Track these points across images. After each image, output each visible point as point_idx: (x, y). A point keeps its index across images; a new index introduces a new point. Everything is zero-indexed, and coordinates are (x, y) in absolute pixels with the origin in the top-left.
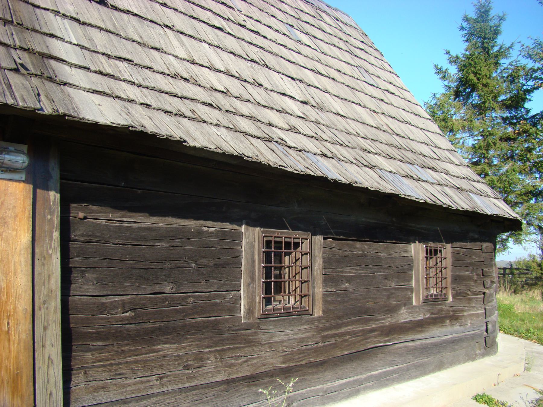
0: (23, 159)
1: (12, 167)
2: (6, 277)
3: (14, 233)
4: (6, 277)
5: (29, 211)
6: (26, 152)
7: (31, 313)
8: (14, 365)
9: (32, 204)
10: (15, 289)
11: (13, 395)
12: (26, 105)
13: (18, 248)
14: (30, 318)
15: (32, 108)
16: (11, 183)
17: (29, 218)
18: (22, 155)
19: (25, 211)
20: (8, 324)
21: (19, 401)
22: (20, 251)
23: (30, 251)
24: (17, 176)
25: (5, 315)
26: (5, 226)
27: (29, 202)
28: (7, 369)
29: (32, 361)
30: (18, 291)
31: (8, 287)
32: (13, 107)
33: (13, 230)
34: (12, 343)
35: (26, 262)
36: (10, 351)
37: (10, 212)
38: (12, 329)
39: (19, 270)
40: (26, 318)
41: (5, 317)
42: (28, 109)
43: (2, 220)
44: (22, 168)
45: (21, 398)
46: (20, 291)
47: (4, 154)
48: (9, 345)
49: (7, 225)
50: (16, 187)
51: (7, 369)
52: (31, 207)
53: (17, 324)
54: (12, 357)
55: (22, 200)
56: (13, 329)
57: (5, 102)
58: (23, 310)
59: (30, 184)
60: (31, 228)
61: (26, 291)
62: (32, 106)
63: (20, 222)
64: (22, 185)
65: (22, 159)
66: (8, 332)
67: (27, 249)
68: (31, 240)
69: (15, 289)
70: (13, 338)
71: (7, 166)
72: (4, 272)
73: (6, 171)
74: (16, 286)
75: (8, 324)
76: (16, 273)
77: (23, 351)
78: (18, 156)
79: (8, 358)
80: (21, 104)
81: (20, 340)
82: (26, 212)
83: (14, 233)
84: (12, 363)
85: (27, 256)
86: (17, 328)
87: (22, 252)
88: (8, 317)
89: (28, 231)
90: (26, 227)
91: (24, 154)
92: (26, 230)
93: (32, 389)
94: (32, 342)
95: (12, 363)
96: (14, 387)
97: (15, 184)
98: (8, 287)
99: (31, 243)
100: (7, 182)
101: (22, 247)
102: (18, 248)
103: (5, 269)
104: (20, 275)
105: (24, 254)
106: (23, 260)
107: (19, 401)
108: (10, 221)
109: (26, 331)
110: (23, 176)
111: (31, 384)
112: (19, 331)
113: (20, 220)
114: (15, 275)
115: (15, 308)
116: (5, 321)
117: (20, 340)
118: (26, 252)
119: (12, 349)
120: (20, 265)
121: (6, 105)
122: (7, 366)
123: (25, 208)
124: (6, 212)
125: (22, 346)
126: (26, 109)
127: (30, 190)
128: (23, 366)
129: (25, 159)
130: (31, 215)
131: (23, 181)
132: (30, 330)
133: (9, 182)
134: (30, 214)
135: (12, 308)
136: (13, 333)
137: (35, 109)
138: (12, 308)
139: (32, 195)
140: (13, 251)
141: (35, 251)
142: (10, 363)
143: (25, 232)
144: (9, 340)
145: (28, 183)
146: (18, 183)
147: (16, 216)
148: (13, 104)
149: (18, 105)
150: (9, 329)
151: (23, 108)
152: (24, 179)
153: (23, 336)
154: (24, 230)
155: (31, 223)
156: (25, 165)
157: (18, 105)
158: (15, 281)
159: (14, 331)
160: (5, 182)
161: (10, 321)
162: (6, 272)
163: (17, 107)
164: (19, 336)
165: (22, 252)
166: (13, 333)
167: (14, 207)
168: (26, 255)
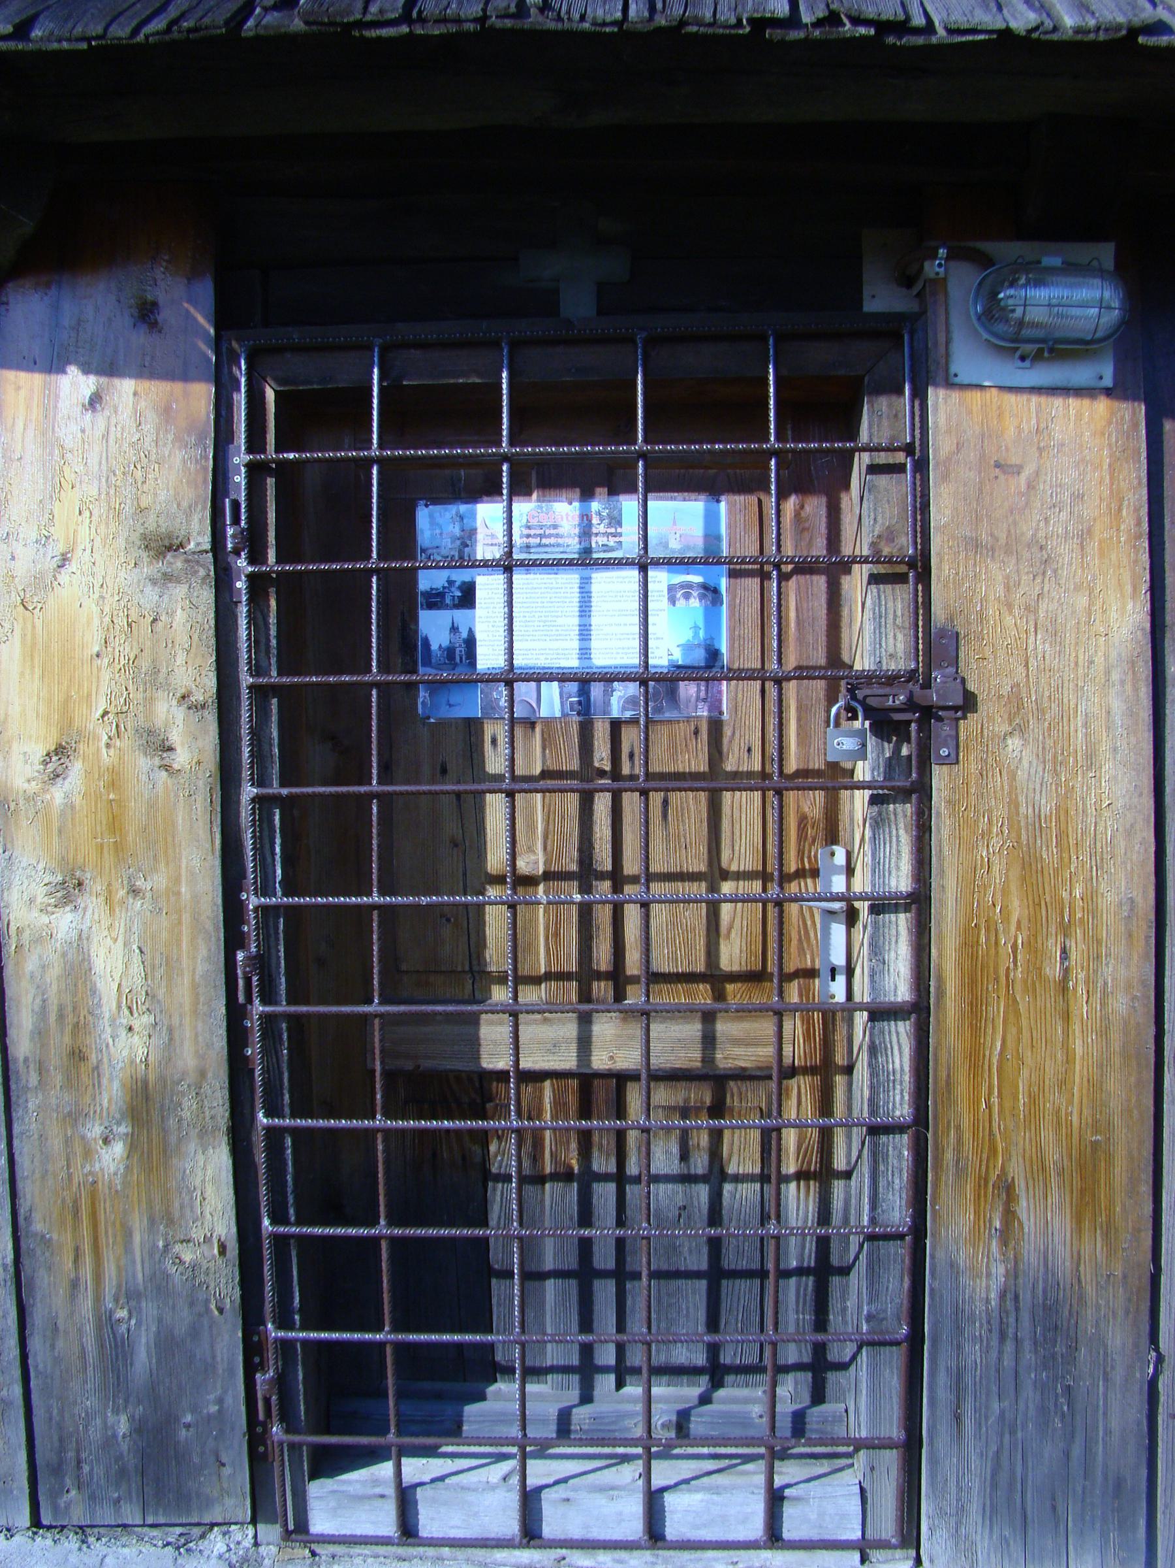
0: (1098, 295)
1: (1057, 335)
2: (1056, 773)
3: (1082, 601)
4: (1056, 773)
5: (1137, 510)
6: (1109, 263)
7: (1152, 917)
8: (1085, 1111)
9: (1145, 480)
10: (1091, 820)
11: (1078, 1219)
12: (1092, 23)
13: (1099, 659)
14: (1147, 938)
15: (1119, 27)
16: (1058, 402)
17: (1138, 537)
18: (1097, 282)
19: (1120, 510)
20: (1064, 952)
21: (1099, 1245)
22: (1108, 672)
23: (1144, 670)
24: (1081, 374)
25: (1054, 917)
26: (1044, 573)
27: (1135, 473)
28: (1059, 1123)
29: (1149, 1101)
30: (1100, 828)
31: (1062, 812)
32: (1038, 40)
33: (1077, 588)
34: (1076, 1027)
35: (1131, 713)
36: (1069, 1058)
37: (1064, 516)
38: (1079, 976)
39: (1104, 747)
40: (1130, 935)
41: (1053, 929)
42: (1102, 37)
43: (1035, 549)
44: (1099, 335)
45: (1106, 1235)
46: (1109, 827)
47: (1023, 281)
48: (1066, 1033)
49: (1055, 571)
50: (1079, 417)
51: (1059, 1123)
52: (1144, 492)
53: (1099, 957)
54: (1077, 1080)
55: (1106, 467)
56: (1081, 976)
57: (1000, 25)
58: (1120, 904)
59: (1135, 398)
60: (1147, 576)
61: (1129, 833)
62: (1121, 19)
63: (1102, 555)
64: (1102, 406)
65: (1097, 294)
66: (1063, 986)
67: (1133, 664)
68: (1148, 626)
69: (1091, 820)
70: (1081, 1008)
71: (1039, 333)
72: (1049, 757)
73: (1038, 357)
74: (1091, 811)
75: (1064, 952)
76: (1091, 757)
77: (1117, 1061)
78: (1079, 286)
79: (1063, 1083)
80: (1069, 21)
81: (1105, 1018)
82: (1124, 512)
83: (1082, 601)
84: (1076, 1100)
85: (1136, 690)
86: (1095, 971)
87: (1115, 676)
88: (1065, 930)
89: (1135, 589)
90: (1127, 577)
91: (1101, 273)
92: (1128, 589)
93: (1148, 1208)
94: (1152, 1031)
95: (1076, 1100)
96: (1082, 1191)
97: (1073, 403)
98: (1062, 812)
99: (1149, 637)
100: (1043, 399)
101: (1113, 655)
102: (1099, 659)
103: (1049, 742)
104: (1108, 768)
105: (1122, 682)
106: (1117, 706)
107: (1099, 1245)
108: (1066, 553)
109: (1129, 986)
110: (1107, 373)
111: (1146, 1189)
112: (1106, 983)
113: (1100, 549)
114: (1089, 768)
115: (1091, 896)
116: (1051, 941)
117: (1105, 1018)
118: (1130, 676)
119: (1079, 1051)
120: (1108, 728)
121: (1006, 34)
122: (1058, 1111)
123: (1121, 500)
124: (1046, 520)
125: (1116, 1046)
126: (1092, 36)
127: (1135, 426)
128: (1117, 1120)
129: (1107, 294)
130: (1145, 526)
131: (1108, 392)
132: (1144, 983)
133: (1050, 399)
134: (1139, 523)
135: (1077, 893)
136: (1081, 989)
137: (1134, 32)
138: (1077, 893)
139: (1144, 445)
140: (1080, 671)
141: (1163, 672)
142: (1070, 1102)
143: (1123, 596)
144: (1066, 1017)
145: (1124, 397)
146: (1086, 402)
147: (1085, 535)
148: (1036, 29)
149: (1055, 29)
150: (1066, 971)
151: (1079, 37)
152: (1108, 382)
153: (1120, 1004)
154: (1120, 585)
155: (1145, 558)
156: (1112, 317)
157: (1055, 29)
158: (1089, 788)
159: (1087, 982)
160: (1034, 399)
161: (1071, 944)
162: (1055, 757)
163: (1055, 37)
164: (1103, 1004)
165: (1115, 676)
166: (1081, 989)
167: (1079, 497)
168: (1129, 687)
